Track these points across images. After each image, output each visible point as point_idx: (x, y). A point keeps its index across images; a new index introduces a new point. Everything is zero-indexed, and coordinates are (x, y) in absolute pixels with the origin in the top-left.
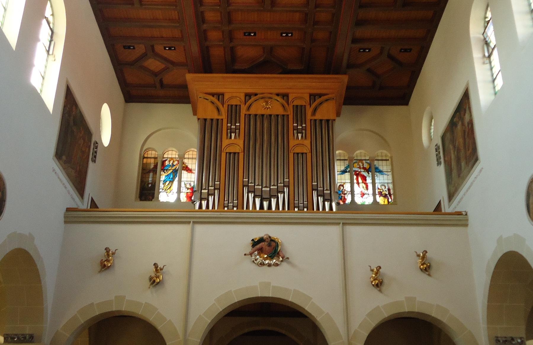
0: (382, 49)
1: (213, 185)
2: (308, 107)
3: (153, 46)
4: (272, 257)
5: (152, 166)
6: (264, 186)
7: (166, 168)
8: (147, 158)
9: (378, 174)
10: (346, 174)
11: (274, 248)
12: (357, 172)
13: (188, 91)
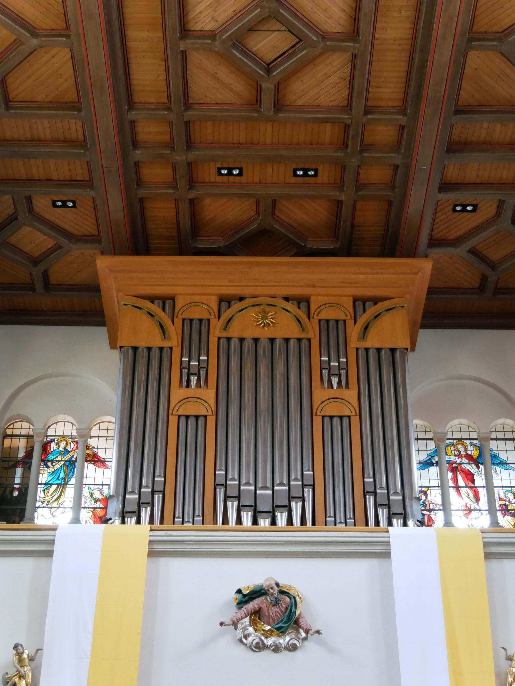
0: (501, 203)
1: (150, 485)
2: (350, 323)
3: (29, 199)
4: (282, 630)
5: (21, 454)
6: (260, 486)
7: (50, 457)
8: (12, 436)
9: (498, 468)
10: (432, 468)
11: (287, 609)
12: (455, 465)
13: (100, 297)
